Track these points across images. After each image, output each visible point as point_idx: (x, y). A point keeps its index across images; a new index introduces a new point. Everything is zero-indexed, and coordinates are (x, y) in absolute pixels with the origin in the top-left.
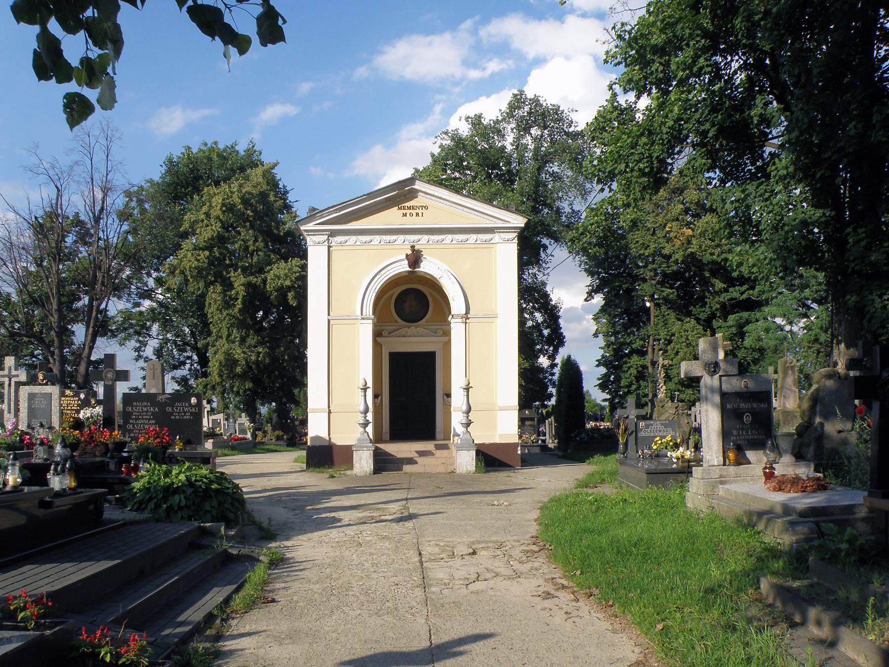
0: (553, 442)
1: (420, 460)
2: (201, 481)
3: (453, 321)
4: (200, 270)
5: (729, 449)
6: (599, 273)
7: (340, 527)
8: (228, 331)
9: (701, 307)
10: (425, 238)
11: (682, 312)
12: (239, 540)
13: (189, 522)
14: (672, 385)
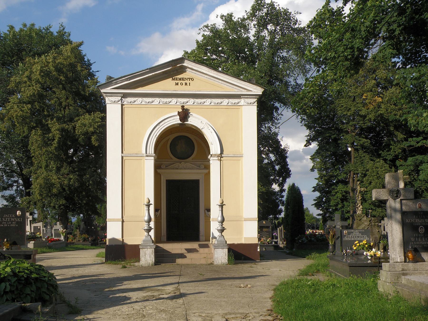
0: (283, 243)
1: (188, 255)
2: (23, 272)
3: (211, 159)
4: (24, 118)
5: (408, 251)
6: (315, 127)
7: (129, 303)
8: (47, 163)
9: (388, 151)
10: (191, 101)
11: (374, 155)
12: (52, 315)
13: (13, 304)
14: (366, 205)
